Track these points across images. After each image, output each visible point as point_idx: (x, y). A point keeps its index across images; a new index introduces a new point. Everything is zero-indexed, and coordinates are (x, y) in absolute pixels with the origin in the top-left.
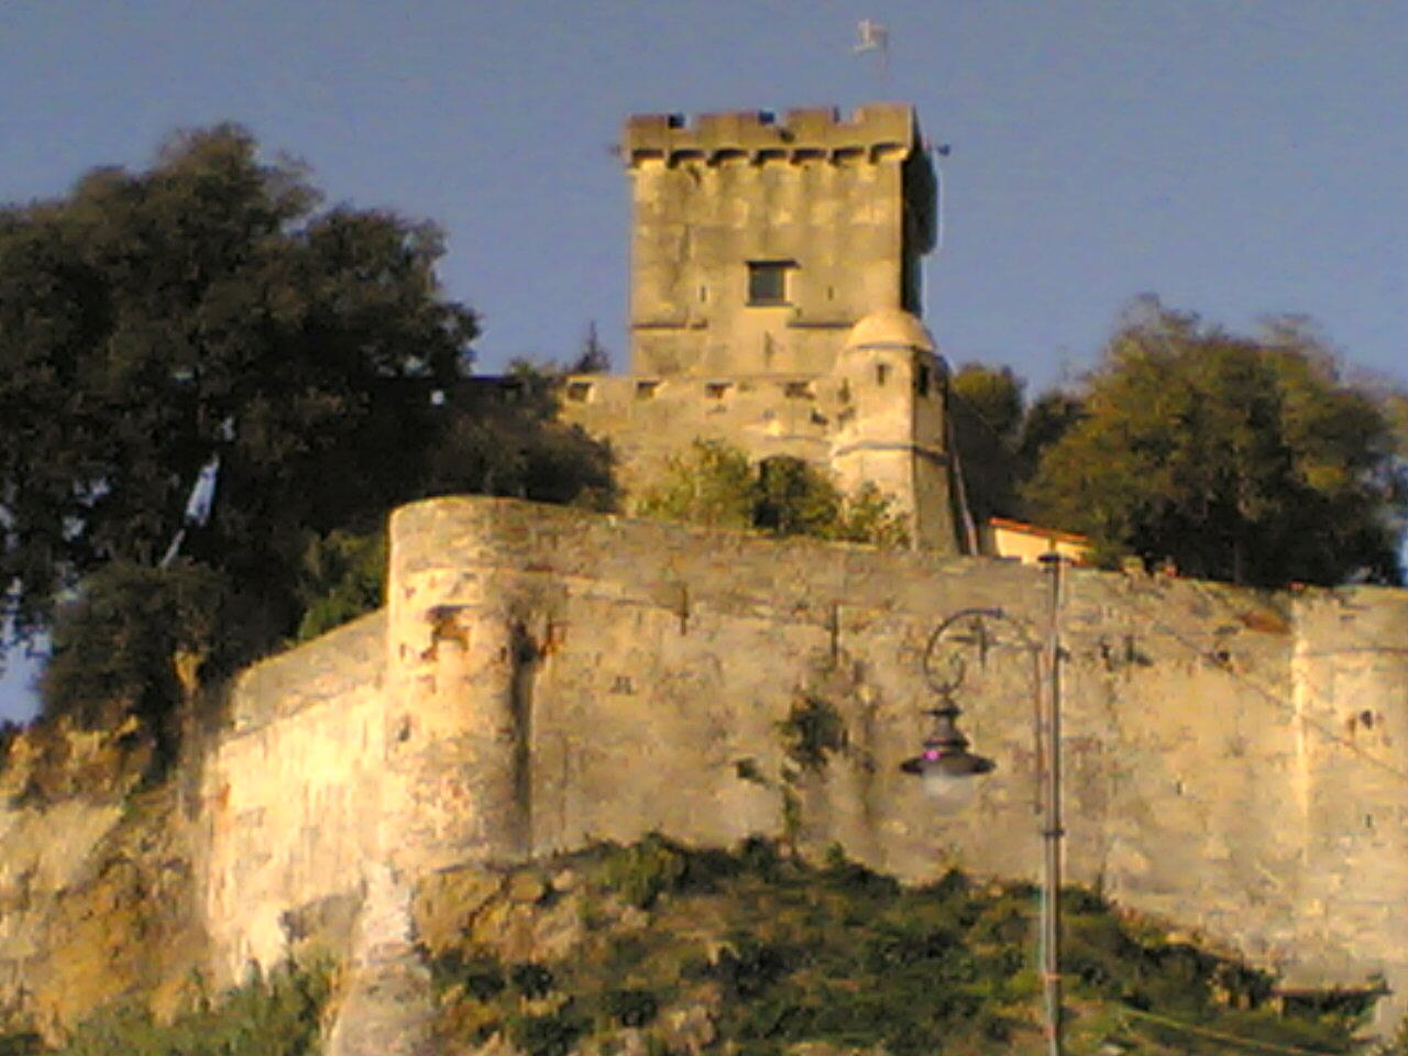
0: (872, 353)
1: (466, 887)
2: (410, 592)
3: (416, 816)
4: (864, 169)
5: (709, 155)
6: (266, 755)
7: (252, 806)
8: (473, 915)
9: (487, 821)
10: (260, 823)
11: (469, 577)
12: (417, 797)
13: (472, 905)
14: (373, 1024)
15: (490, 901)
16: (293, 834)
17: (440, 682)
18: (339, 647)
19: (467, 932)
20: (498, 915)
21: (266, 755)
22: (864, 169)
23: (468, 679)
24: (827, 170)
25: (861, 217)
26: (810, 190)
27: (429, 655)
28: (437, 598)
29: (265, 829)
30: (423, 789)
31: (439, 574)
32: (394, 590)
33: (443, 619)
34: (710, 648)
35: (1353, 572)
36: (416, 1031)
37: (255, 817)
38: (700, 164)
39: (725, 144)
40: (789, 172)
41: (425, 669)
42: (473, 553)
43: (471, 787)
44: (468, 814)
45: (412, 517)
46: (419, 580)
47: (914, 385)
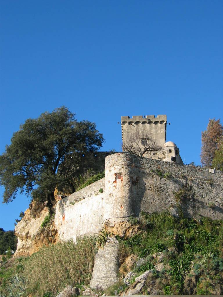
0: (168, 148)
1: (124, 225)
2: (110, 171)
3: (114, 212)
4: (159, 125)
5: (134, 122)
6: (72, 210)
7: (70, 219)
8: (126, 230)
9: (128, 213)
10: (71, 221)
11: (123, 167)
12: (114, 208)
13: (126, 228)
14: (107, 252)
15: (129, 228)
16: (78, 223)
17: (117, 187)
18: (87, 189)
19: (125, 233)
20: (131, 230)
21: (72, 210)
22: (159, 125)
23: (124, 186)
24: (153, 125)
25: (159, 132)
26: (151, 128)
27: (115, 182)
28: (116, 171)
29: (72, 223)
30: (115, 207)
31: (116, 167)
32: (106, 172)
33: (118, 175)
34: (165, 182)
35: (139, 227)
36: (116, 252)
37: (70, 221)
38: (133, 124)
39: (137, 121)
40: (147, 125)
41: (114, 184)
42: (123, 163)
43: (124, 206)
44: (124, 211)
45: (110, 157)
46: (112, 168)
47: (175, 153)
